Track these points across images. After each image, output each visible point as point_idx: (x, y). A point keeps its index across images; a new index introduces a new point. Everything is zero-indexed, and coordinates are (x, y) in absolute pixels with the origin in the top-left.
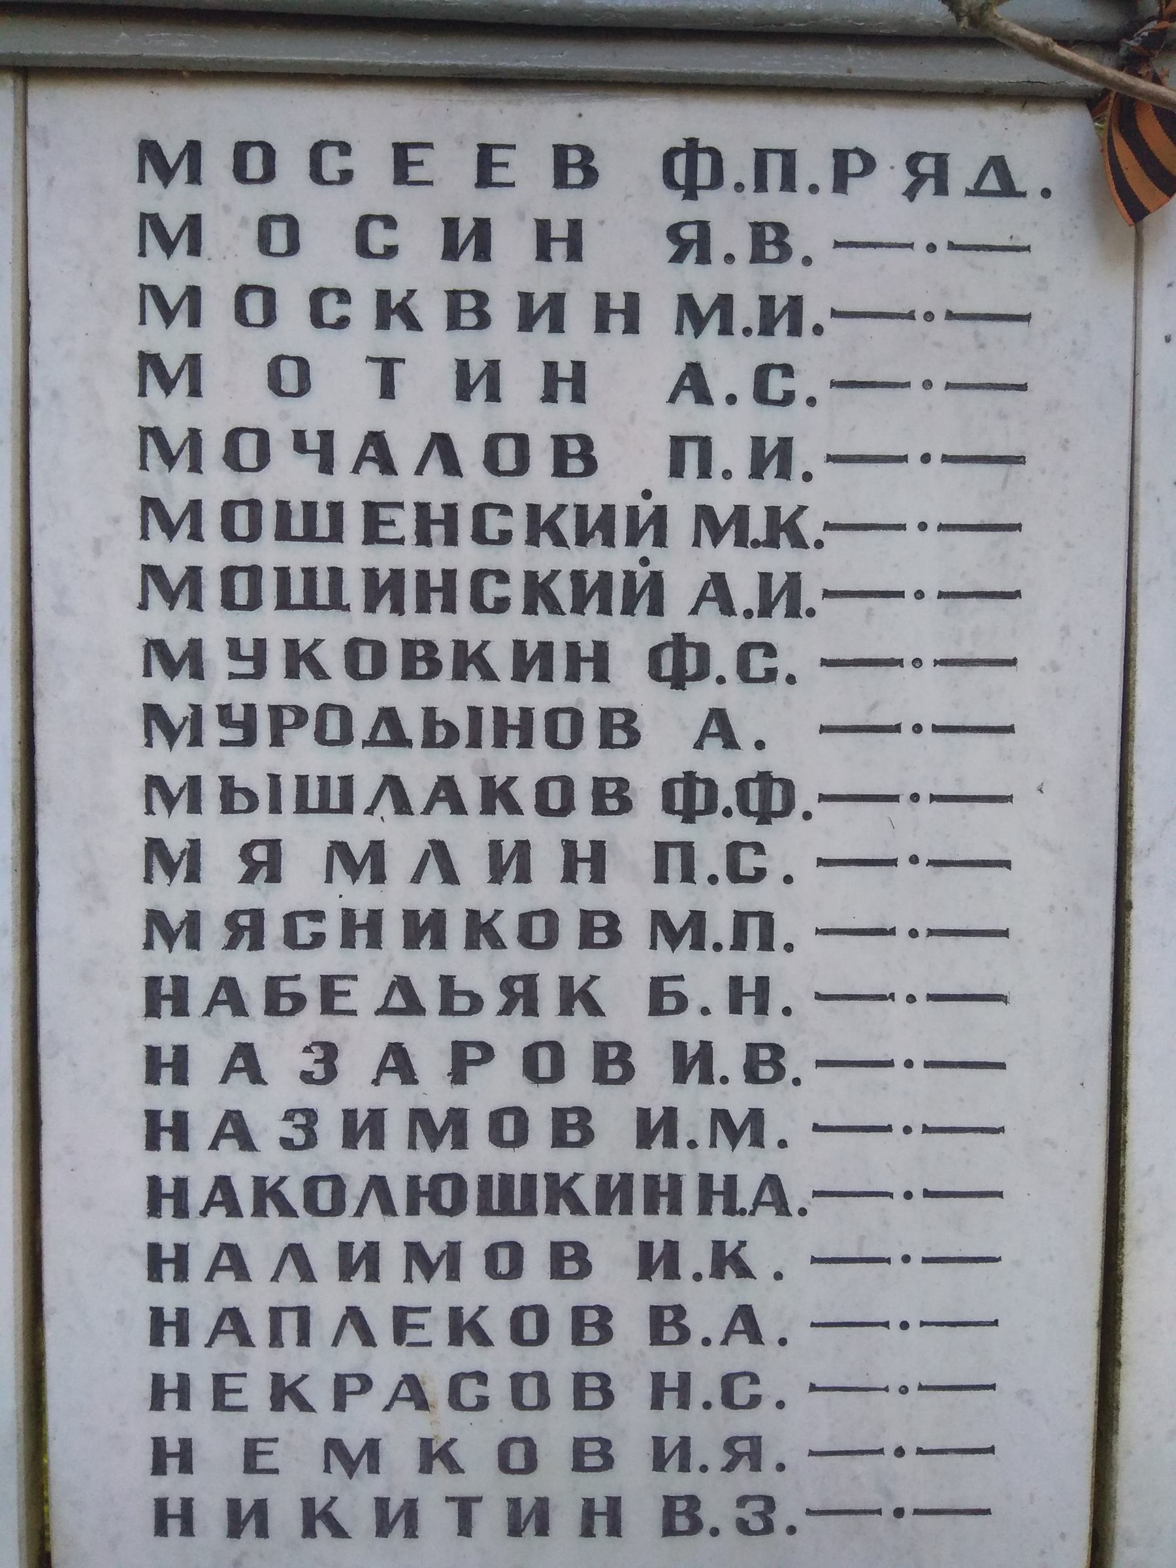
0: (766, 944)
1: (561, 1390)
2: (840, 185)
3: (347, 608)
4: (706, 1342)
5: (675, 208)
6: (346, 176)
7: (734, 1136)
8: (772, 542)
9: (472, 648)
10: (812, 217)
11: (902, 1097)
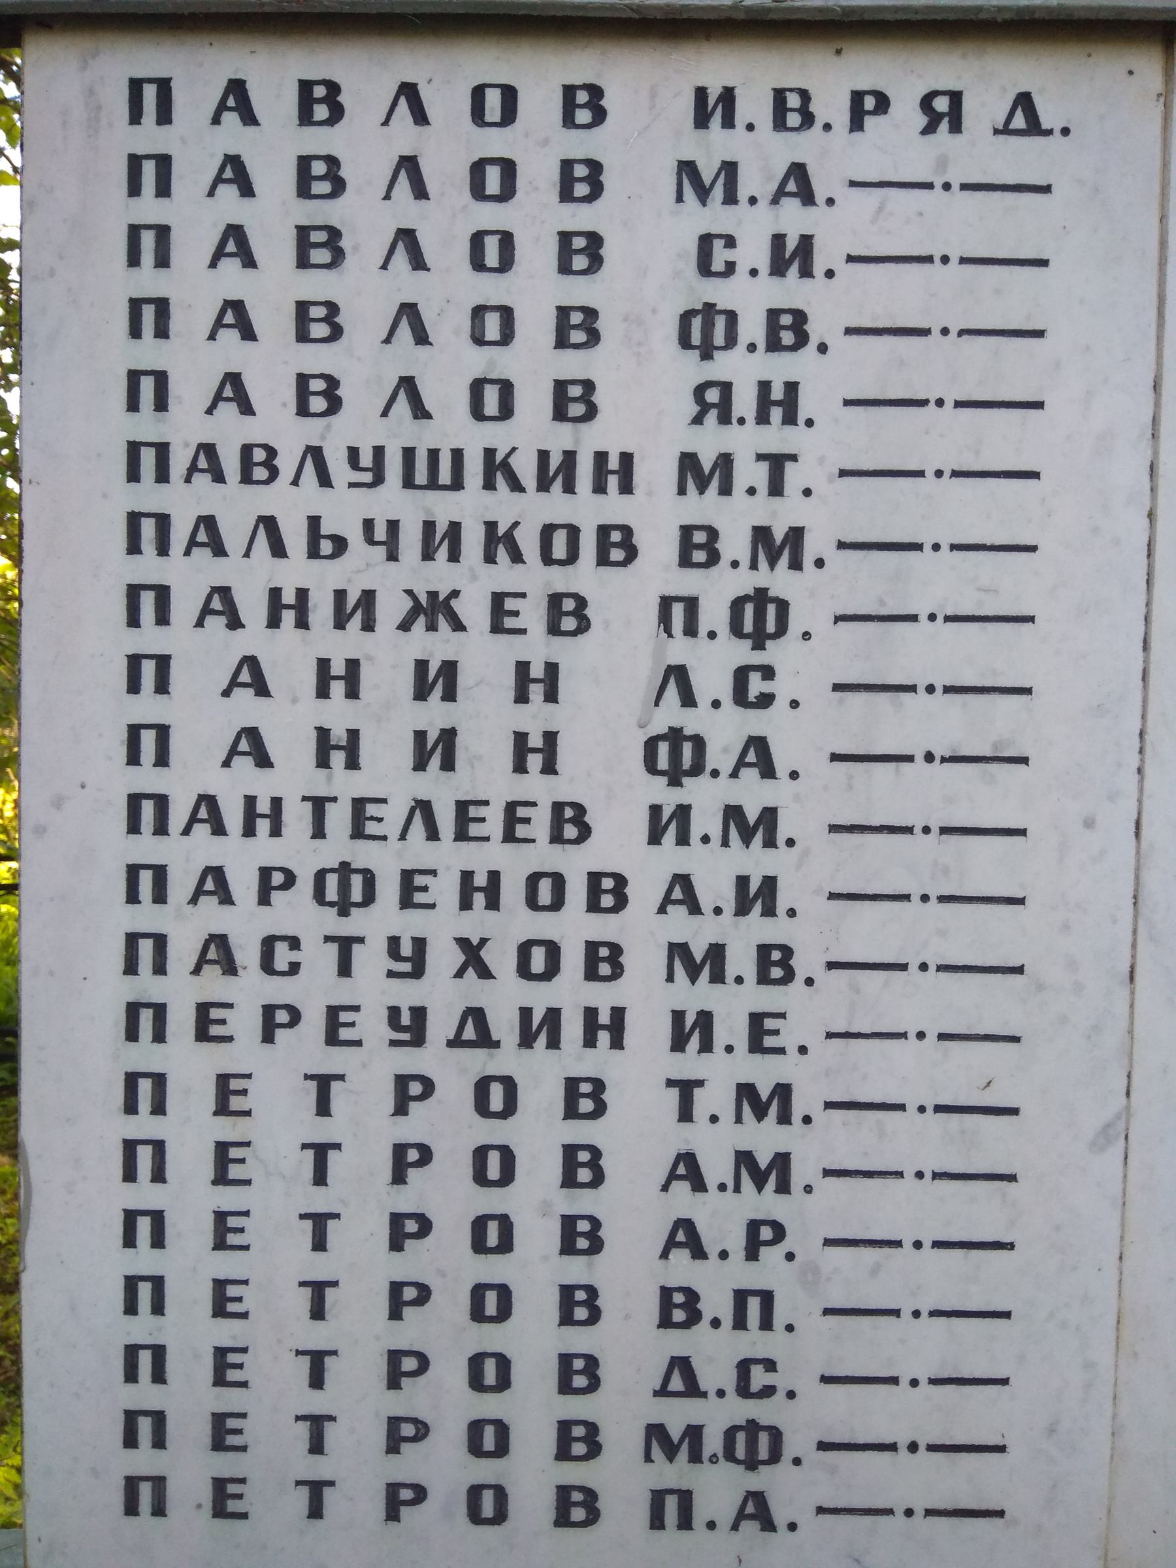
0: (766, 1324)
1: (573, 960)
3: (497, 1045)
4: (718, 911)
5: (693, 369)
6: (294, 968)
7: (747, 837)
8: (779, 268)
10: (832, 155)
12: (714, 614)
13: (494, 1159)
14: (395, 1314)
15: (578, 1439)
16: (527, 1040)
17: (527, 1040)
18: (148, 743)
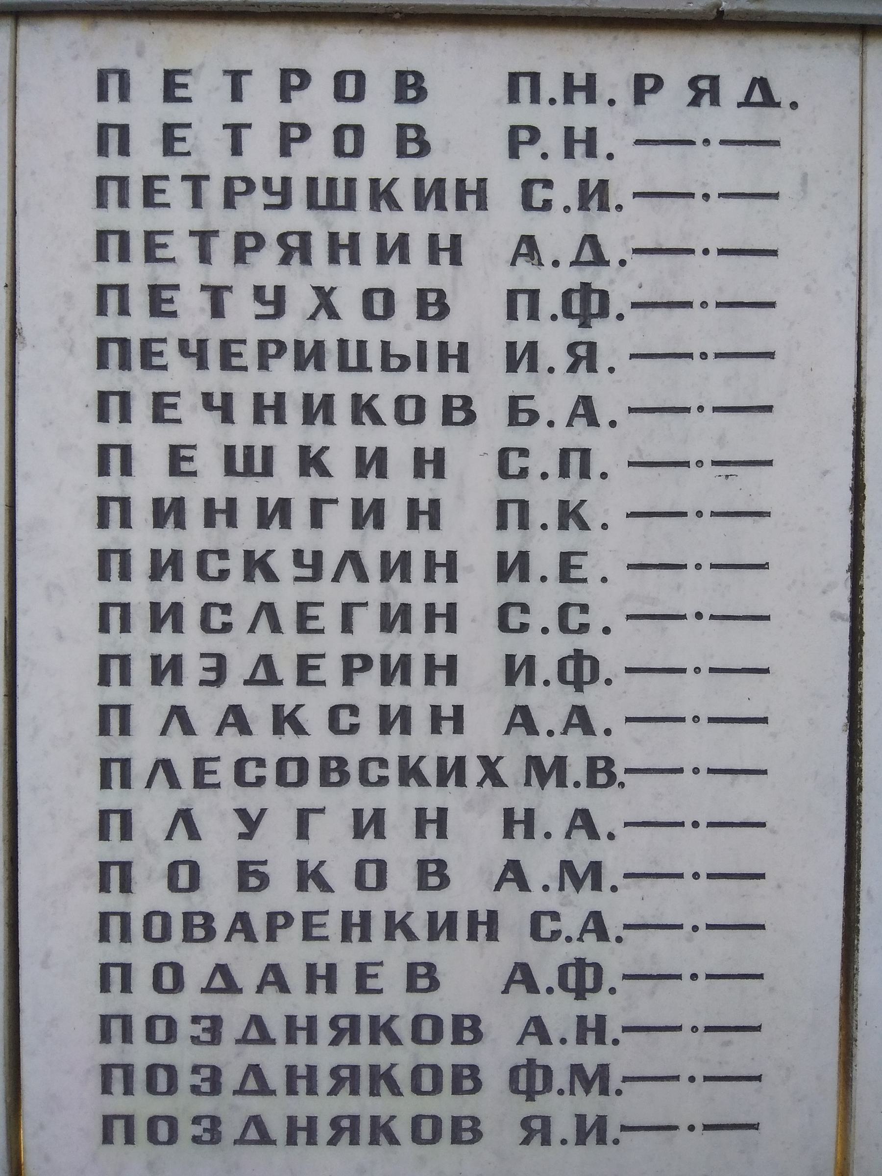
0: (585, 473)
2: (639, 99)
7: (587, 1087)
8: (581, 1139)
9: (398, 918)
11: (692, 695)
12: (550, 303)
13: (378, 298)
14: (285, 98)
15: (466, 1130)
16: (433, 935)
17: (433, 935)
18: (116, 875)
